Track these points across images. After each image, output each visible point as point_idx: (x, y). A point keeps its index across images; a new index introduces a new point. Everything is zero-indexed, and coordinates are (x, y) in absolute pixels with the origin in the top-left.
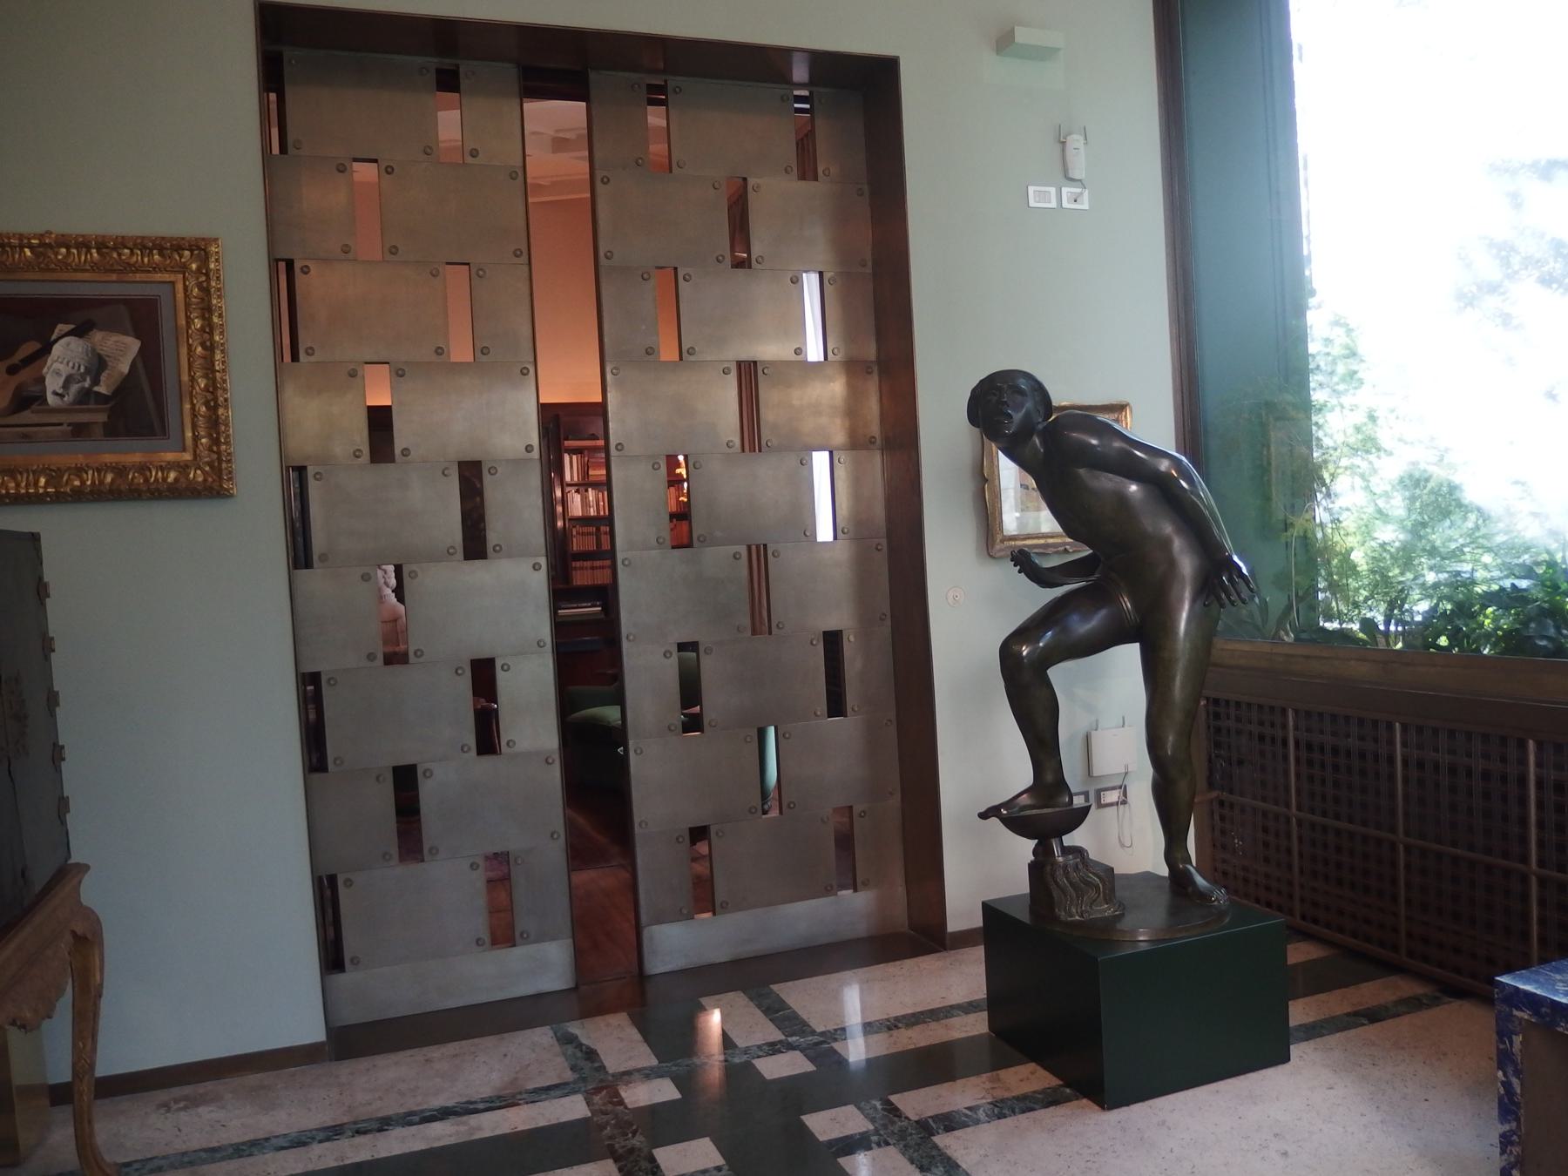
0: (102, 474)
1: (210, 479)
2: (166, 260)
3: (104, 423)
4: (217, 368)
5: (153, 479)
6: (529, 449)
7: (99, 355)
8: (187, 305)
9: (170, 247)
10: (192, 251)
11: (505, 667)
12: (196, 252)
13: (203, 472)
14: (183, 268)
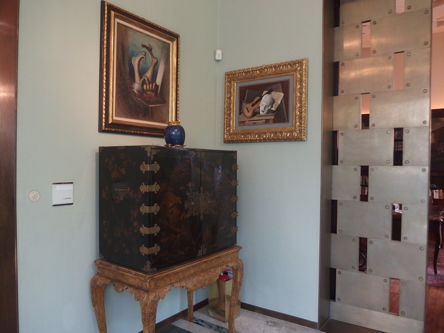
0: (271, 134)
1: (299, 135)
2: (291, 68)
3: (273, 119)
4: (303, 100)
5: (283, 135)
6: (425, 122)
7: (273, 99)
8: (296, 81)
9: (292, 64)
10: (299, 64)
11: (406, 208)
12: (300, 64)
13: (297, 133)
14: (296, 70)
